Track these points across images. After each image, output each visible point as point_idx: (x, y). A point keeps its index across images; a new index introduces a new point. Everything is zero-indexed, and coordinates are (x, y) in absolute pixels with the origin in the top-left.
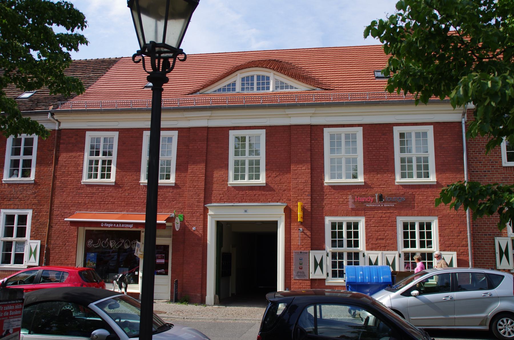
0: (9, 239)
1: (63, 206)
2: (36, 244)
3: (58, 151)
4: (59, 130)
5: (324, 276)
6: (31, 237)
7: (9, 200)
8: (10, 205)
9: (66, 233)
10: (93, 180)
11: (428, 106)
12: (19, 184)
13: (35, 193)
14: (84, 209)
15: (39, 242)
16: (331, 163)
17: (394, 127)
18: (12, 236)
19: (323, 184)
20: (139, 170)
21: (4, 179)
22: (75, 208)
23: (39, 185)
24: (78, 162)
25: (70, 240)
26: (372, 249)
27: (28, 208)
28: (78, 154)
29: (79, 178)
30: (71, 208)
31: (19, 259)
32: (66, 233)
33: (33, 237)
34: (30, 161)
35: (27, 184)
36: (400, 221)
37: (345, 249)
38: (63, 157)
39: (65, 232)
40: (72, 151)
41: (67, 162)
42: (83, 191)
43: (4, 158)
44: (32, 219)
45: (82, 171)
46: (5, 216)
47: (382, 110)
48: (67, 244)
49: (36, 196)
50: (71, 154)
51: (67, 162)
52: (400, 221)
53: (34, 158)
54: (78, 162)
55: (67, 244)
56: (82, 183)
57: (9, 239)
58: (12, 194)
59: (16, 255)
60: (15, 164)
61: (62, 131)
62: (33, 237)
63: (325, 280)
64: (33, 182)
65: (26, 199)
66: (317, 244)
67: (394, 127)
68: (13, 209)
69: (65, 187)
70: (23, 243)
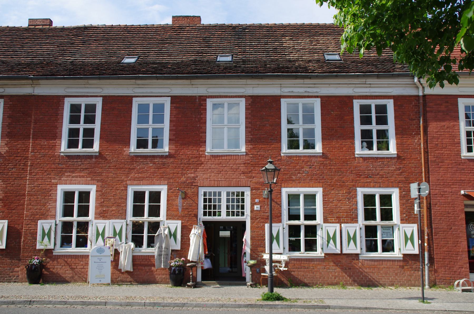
0: (372, 223)
1: (442, 184)
2: (412, 229)
3: (425, 121)
4: (424, 96)
5: (358, 251)
6: (401, 220)
7: (367, 177)
8: (370, 182)
9: (450, 215)
10: (142, 151)
11: (471, 79)
12: (377, 158)
13: (399, 169)
14: (470, 187)
15: (6, 222)
16: (467, 136)
17: (459, 99)
18: (72, 216)
19: (354, 154)
20: (280, 141)
21: (357, 152)
22: (457, 186)
23: (404, 159)
24: (453, 133)
25: (456, 223)
26: (170, 219)
27: (393, 187)
28: (452, 124)
29: (458, 151)
30: (452, 186)
31: (388, 246)
32: (450, 215)
33: (169, 217)
34: (93, 130)
35: (387, 158)
36: (361, 192)
37: (302, 222)
38: (433, 127)
39: (449, 213)
40: (443, 120)
41: (439, 133)
42: (465, 167)
43: (353, 127)
44: (401, 199)
45: (459, 143)
46: (363, 196)
47: (70, 83)
48: (453, 228)
49: (401, 173)
50: (443, 124)
51: (439, 133)
52: (285, 191)
53: (97, 127)
54: (453, 133)
55: (453, 228)
56: (462, 158)
57: (372, 223)
58: (370, 170)
59: (384, 242)
60: (73, 133)
61: (427, 97)
62: (169, 217)
63: (357, 255)
64: (396, 156)
65: (388, 175)
66: (275, 217)
67: (459, 99)
68: (373, 187)
69: (442, 162)
70: (392, 228)
